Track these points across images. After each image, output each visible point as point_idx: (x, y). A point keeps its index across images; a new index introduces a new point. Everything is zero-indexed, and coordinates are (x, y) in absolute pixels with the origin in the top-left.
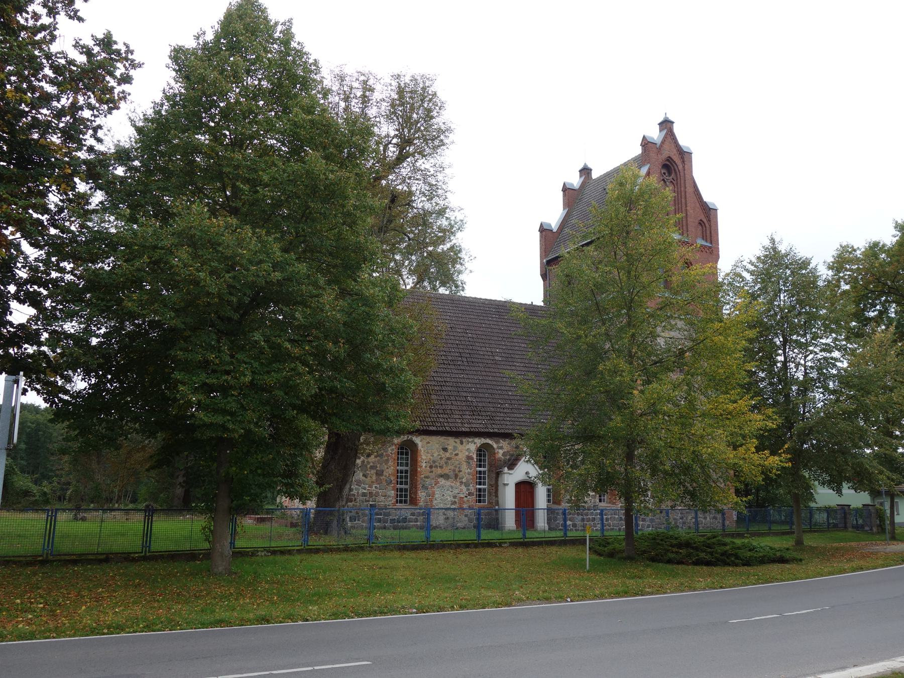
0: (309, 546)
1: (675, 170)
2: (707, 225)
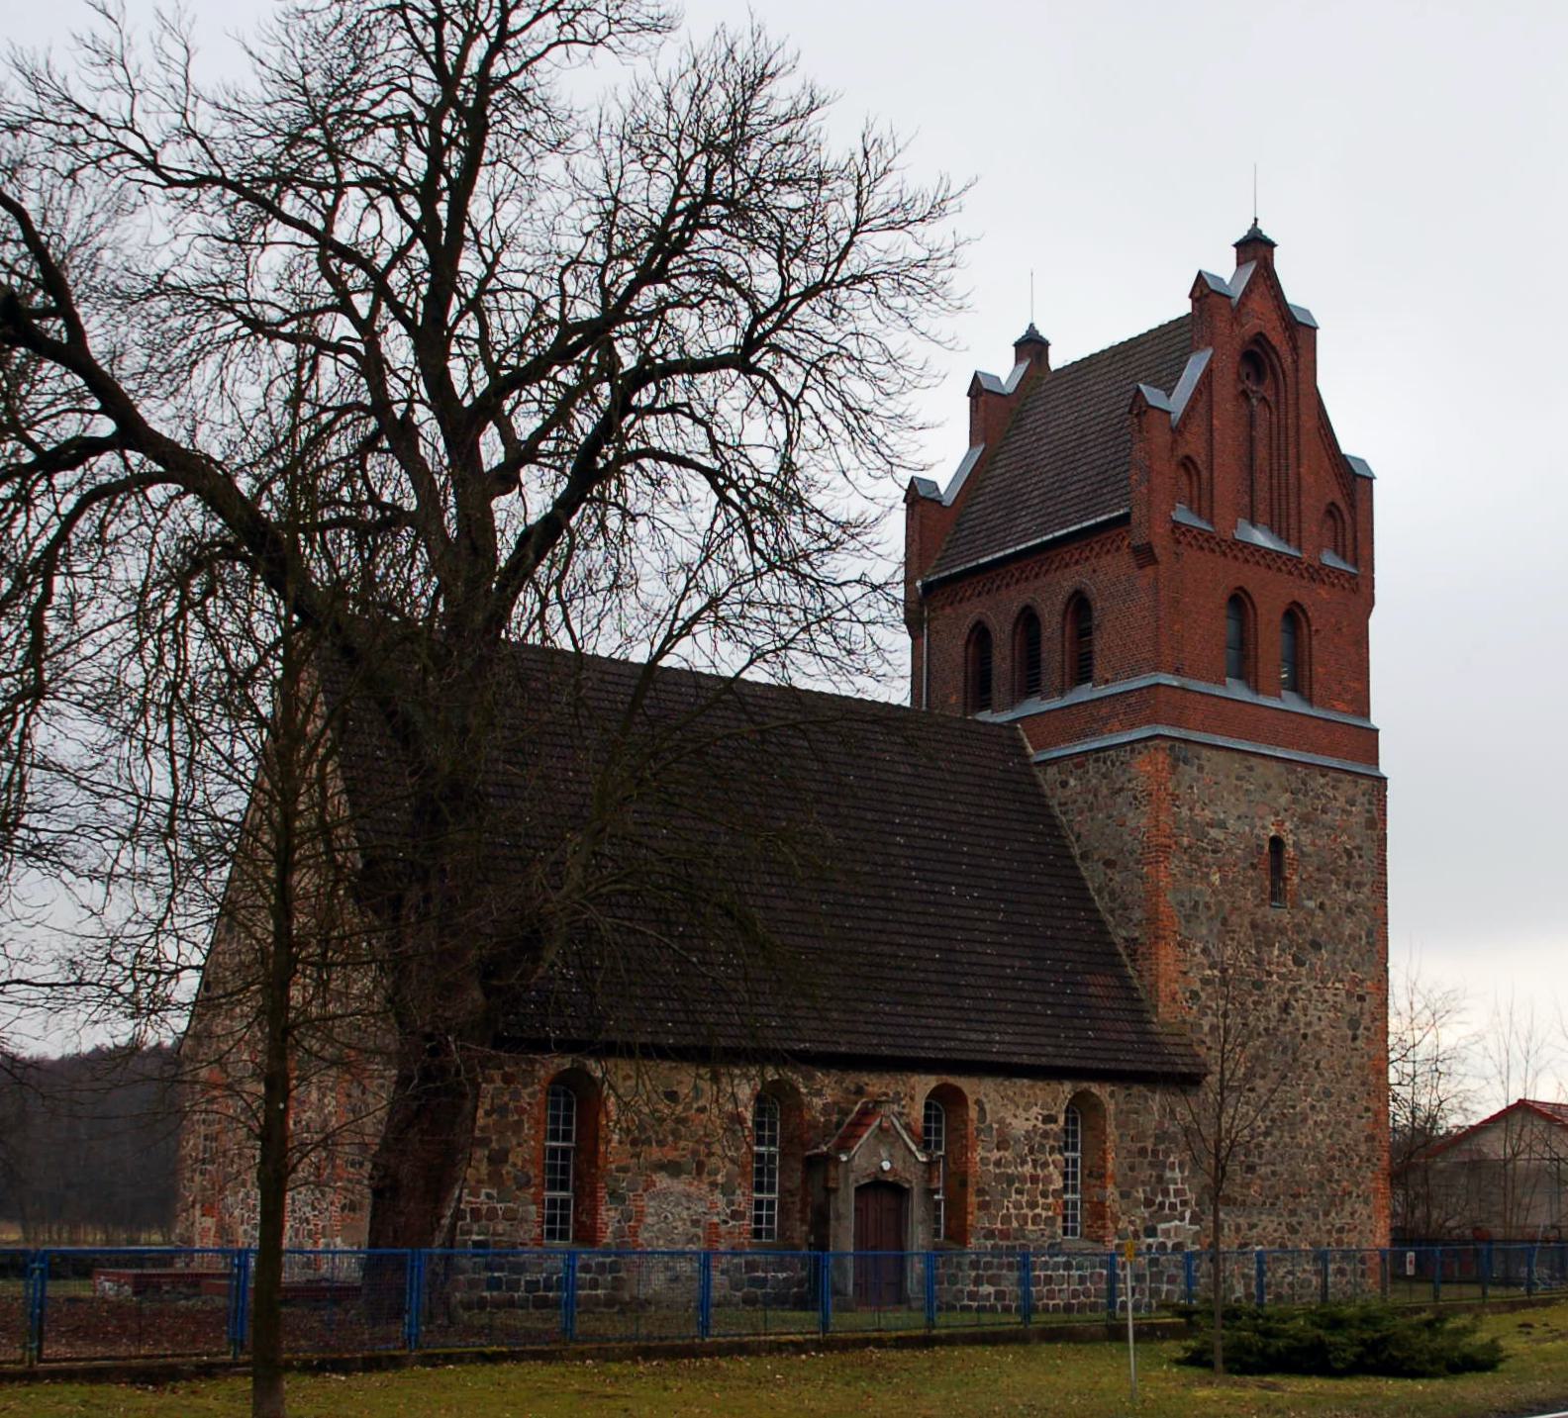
1: (1272, 367)
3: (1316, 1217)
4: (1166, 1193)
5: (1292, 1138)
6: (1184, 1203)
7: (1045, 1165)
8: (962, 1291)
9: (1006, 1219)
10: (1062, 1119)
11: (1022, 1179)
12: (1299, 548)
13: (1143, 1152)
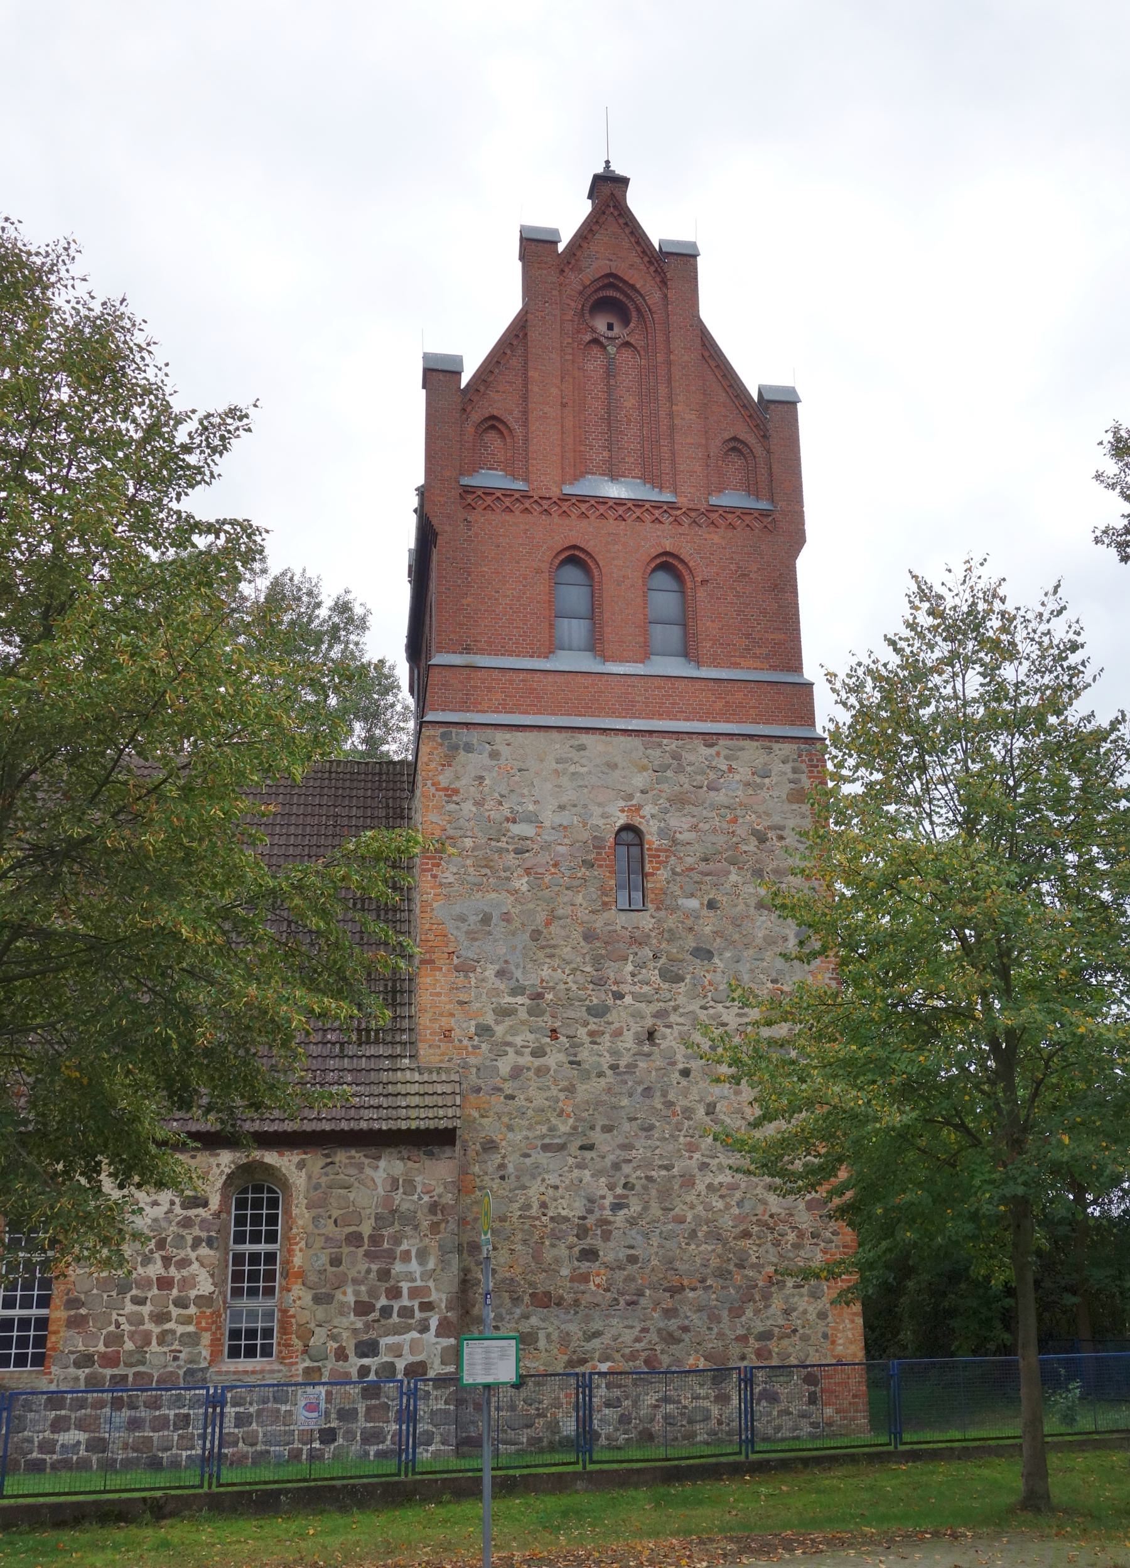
0: (399, 1470)
1: (638, 310)
2: (759, 451)
3: (714, 1318)
4: (394, 1293)
5: (666, 1210)
6: (427, 1307)
7: (184, 1263)
8: (30, 1440)
9: (115, 1339)
10: (215, 1202)
11: (145, 1283)
12: (675, 492)
13: (355, 1239)
